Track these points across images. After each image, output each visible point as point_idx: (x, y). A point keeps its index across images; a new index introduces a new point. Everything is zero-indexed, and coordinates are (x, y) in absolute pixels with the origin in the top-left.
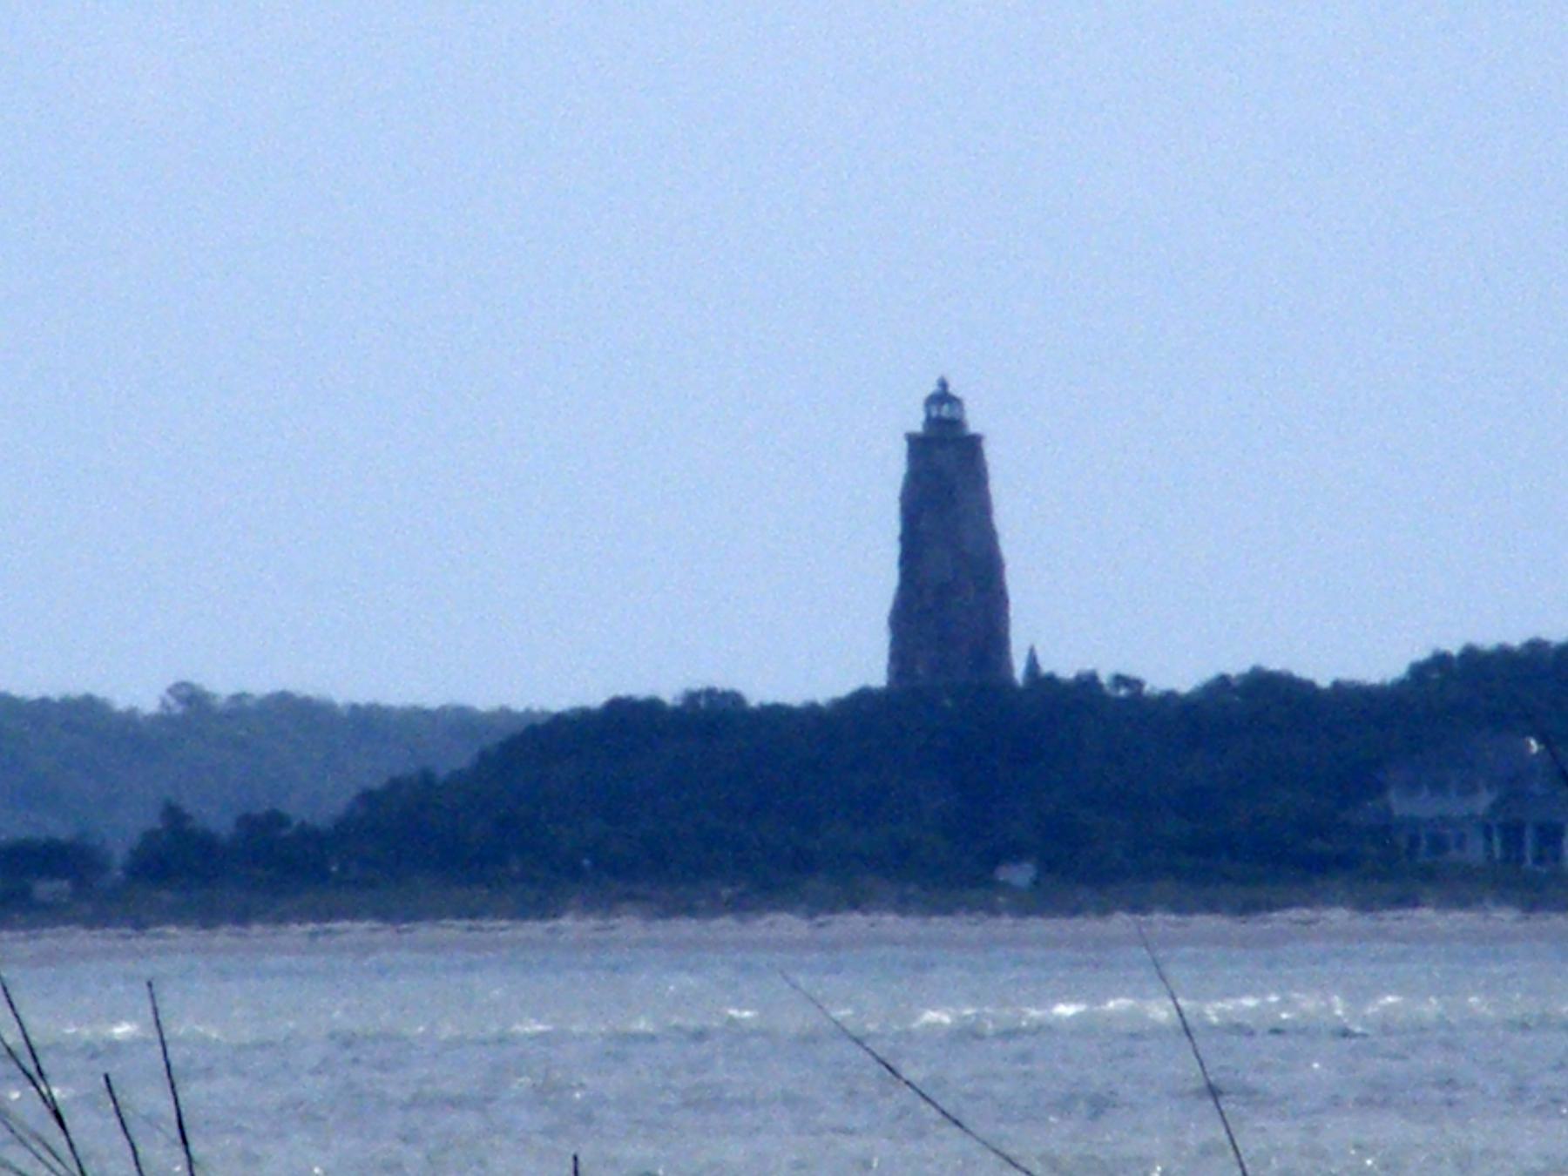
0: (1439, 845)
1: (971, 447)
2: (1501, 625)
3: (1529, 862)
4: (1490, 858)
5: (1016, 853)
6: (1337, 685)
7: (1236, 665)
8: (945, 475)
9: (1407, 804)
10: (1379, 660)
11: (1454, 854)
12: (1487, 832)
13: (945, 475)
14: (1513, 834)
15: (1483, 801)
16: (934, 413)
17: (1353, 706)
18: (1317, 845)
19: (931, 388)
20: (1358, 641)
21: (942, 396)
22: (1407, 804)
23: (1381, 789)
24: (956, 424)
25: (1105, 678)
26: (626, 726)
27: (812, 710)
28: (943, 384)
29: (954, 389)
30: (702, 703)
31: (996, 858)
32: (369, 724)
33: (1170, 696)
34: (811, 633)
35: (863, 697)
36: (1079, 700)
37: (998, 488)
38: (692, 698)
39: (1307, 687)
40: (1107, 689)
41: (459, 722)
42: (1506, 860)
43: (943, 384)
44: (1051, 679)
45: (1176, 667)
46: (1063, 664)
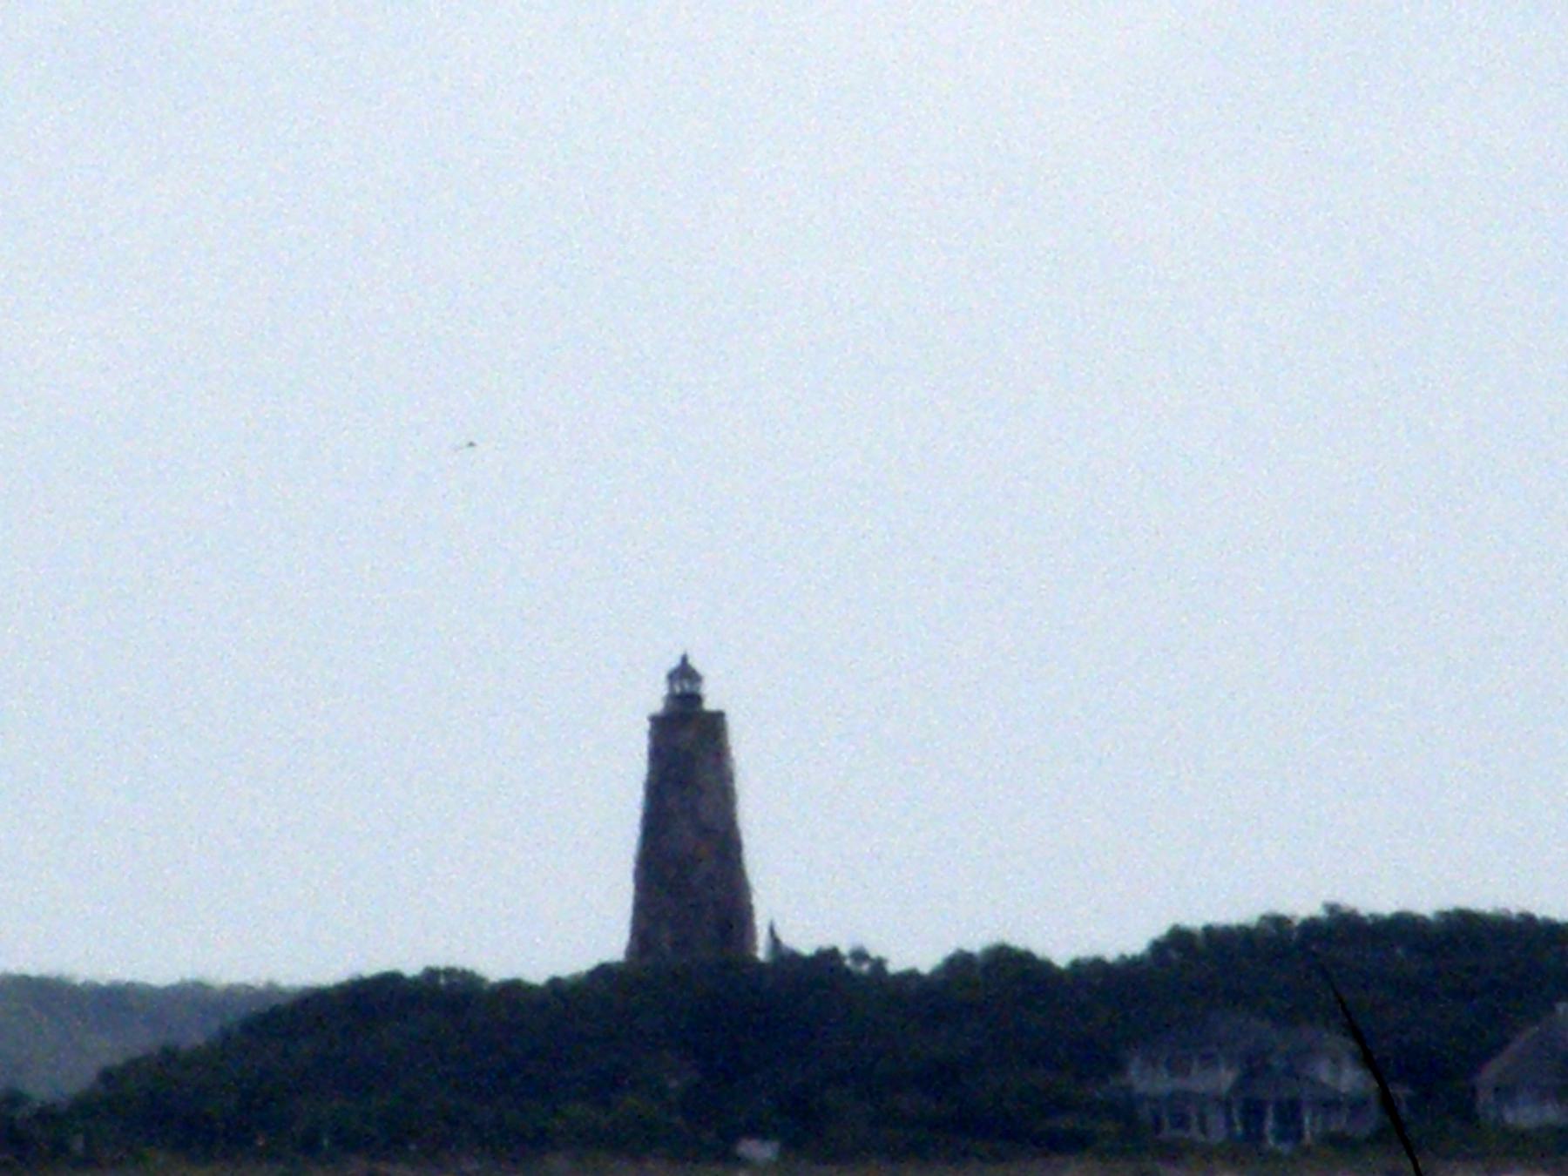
0: (1181, 1122)
1: (714, 726)
2: (1228, 898)
3: (1271, 1142)
4: (1231, 1135)
5: (756, 1130)
6: (1076, 964)
7: (976, 942)
8: (688, 750)
9: (1146, 1079)
10: (1124, 934)
11: (1195, 1132)
12: (1227, 1104)
13: (688, 750)
14: (1254, 1112)
15: (1225, 1078)
16: (678, 689)
17: (1096, 978)
18: (1065, 1122)
19: (674, 662)
20: (1093, 918)
21: (684, 673)
22: (1146, 1079)
23: (1118, 1066)
24: (694, 699)
25: (844, 950)
26: (374, 1003)
27: (513, 991)
28: (684, 659)
29: (696, 663)
30: (442, 981)
31: (731, 1137)
32: (114, 1003)
33: (911, 976)
34: (561, 915)
35: (603, 972)
36: (828, 980)
37: (1378, 898)
38: (431, 974)
39: (1046, 967)
40: (848, 962)
41: (192, 998)
42: (1248, 1136)
43: (684, 659)
44: (794, 957)
45: (914, 947)
46: (804, 941)
